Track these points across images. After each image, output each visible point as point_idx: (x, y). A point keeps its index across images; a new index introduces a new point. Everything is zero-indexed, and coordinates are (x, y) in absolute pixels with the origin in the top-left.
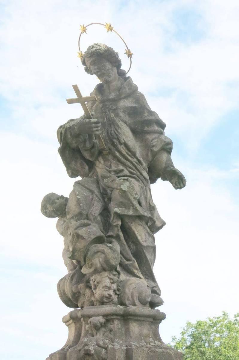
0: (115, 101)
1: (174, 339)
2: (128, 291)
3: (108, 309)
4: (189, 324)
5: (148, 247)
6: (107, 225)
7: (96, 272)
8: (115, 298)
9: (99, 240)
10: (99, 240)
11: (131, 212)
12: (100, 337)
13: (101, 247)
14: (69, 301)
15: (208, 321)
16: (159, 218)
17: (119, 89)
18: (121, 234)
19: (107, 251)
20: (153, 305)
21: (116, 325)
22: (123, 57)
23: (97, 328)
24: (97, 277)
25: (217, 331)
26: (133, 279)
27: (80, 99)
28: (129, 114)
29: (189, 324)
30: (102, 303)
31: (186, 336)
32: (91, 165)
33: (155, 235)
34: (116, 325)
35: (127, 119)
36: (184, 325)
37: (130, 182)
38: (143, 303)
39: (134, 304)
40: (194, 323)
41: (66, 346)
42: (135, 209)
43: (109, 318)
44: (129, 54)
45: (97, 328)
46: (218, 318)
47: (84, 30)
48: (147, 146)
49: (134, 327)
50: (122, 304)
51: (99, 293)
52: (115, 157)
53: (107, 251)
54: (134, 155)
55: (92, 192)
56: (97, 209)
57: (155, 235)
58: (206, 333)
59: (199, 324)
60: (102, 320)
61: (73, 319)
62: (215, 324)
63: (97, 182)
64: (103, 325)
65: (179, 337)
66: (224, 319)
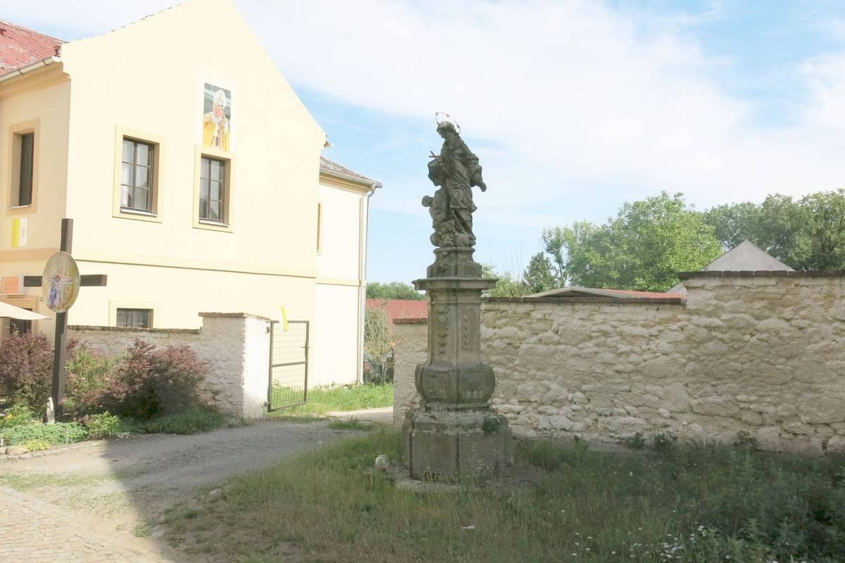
0: (453, 150)
1: (610, 220)
2: (458, 241)
3: (449, 249)
4: (626, 205)
5: (468, 221)
6: (448, 213)
7: (444, 233)
8: (452, 244)
9: (445, 220)
10: (445, 220)
11: (458, 207)
12: (445, 261)
13: (445, 223)
14: (435, 243)
15: (647, 201)
16: (474, 205)
17: (455, 144)
18: (455, 216)
19: (447, 225)
20: (471, 245)
21: (453, 255)
22: (456, 127)
23: (444, 257)
24: (443, 236)
25: (655, 212)
26: (461, 235)
27: (434, 156)
28: (460, 156)
29: (626, 205)
30: (447, 246)
31: (623, 216)
32: (444, 181)
33: (472, 214)
34: (453, 255)
35: (459, 158)
36: (622, 206)
37: (459, 192)
38: (466, 245)
39: (461, 246)
40: (632, 203)
41: (385, 288)
42: (460, 206)
43: (449, 253)
44: (459, 127)
45: (444, 257)
46: (656, 199)
47: (437, 114)
48: (469, 171)
49: (460, 256)
50: (456, 246)
51: (445, 242)
52: (454, 178)
53: (447, 225)
54: (462, 176)
55: (443, 196)
56: (444, 205)
57: (472, 214)
58: (644, 213)
59: (637, 205)
60: (446, 253)
61: (436, 252)
62: (654, 205)
63: (193, 515)
64: (447, 255)
65: (615, 218)
66: (663, 200)
